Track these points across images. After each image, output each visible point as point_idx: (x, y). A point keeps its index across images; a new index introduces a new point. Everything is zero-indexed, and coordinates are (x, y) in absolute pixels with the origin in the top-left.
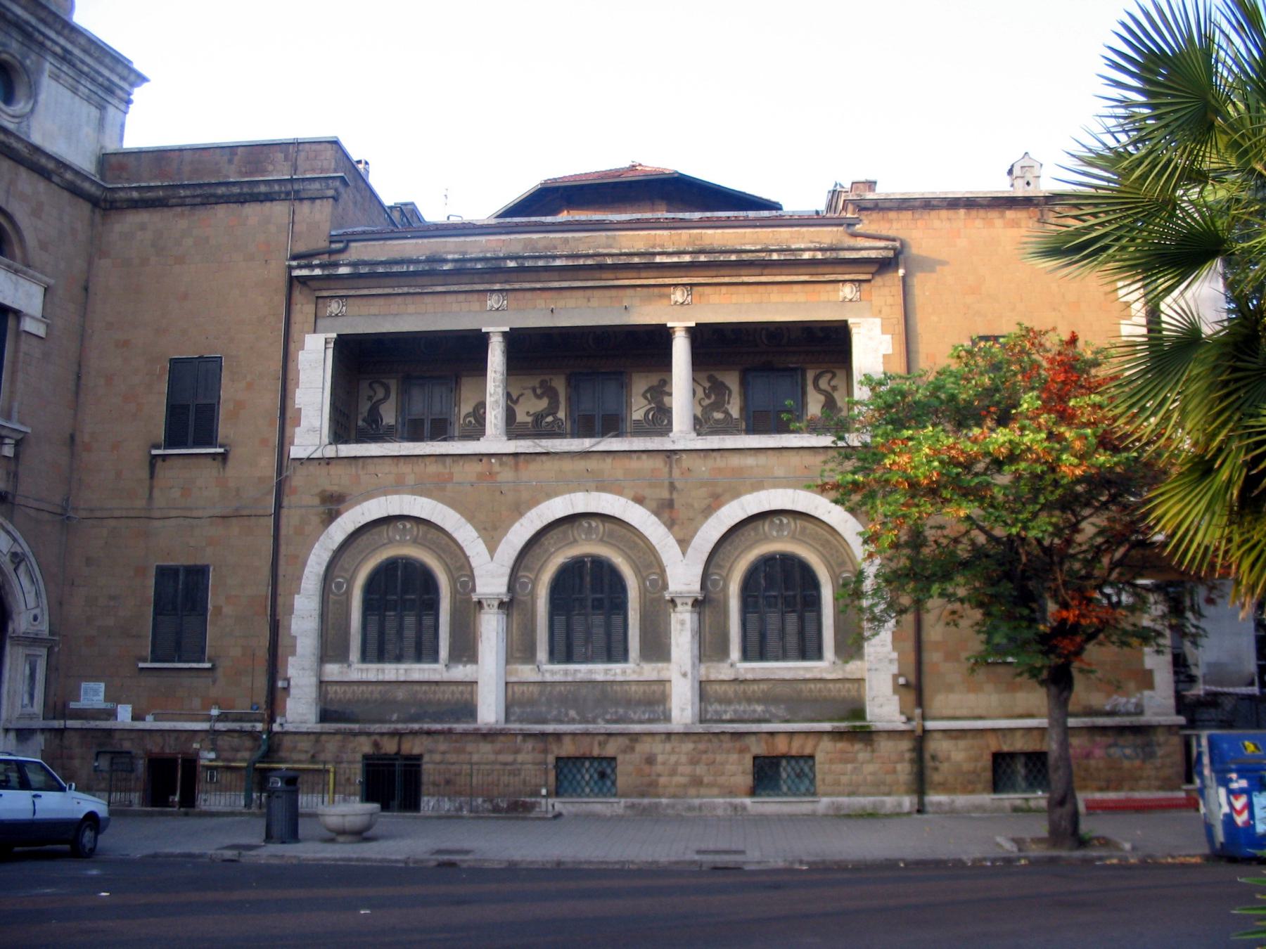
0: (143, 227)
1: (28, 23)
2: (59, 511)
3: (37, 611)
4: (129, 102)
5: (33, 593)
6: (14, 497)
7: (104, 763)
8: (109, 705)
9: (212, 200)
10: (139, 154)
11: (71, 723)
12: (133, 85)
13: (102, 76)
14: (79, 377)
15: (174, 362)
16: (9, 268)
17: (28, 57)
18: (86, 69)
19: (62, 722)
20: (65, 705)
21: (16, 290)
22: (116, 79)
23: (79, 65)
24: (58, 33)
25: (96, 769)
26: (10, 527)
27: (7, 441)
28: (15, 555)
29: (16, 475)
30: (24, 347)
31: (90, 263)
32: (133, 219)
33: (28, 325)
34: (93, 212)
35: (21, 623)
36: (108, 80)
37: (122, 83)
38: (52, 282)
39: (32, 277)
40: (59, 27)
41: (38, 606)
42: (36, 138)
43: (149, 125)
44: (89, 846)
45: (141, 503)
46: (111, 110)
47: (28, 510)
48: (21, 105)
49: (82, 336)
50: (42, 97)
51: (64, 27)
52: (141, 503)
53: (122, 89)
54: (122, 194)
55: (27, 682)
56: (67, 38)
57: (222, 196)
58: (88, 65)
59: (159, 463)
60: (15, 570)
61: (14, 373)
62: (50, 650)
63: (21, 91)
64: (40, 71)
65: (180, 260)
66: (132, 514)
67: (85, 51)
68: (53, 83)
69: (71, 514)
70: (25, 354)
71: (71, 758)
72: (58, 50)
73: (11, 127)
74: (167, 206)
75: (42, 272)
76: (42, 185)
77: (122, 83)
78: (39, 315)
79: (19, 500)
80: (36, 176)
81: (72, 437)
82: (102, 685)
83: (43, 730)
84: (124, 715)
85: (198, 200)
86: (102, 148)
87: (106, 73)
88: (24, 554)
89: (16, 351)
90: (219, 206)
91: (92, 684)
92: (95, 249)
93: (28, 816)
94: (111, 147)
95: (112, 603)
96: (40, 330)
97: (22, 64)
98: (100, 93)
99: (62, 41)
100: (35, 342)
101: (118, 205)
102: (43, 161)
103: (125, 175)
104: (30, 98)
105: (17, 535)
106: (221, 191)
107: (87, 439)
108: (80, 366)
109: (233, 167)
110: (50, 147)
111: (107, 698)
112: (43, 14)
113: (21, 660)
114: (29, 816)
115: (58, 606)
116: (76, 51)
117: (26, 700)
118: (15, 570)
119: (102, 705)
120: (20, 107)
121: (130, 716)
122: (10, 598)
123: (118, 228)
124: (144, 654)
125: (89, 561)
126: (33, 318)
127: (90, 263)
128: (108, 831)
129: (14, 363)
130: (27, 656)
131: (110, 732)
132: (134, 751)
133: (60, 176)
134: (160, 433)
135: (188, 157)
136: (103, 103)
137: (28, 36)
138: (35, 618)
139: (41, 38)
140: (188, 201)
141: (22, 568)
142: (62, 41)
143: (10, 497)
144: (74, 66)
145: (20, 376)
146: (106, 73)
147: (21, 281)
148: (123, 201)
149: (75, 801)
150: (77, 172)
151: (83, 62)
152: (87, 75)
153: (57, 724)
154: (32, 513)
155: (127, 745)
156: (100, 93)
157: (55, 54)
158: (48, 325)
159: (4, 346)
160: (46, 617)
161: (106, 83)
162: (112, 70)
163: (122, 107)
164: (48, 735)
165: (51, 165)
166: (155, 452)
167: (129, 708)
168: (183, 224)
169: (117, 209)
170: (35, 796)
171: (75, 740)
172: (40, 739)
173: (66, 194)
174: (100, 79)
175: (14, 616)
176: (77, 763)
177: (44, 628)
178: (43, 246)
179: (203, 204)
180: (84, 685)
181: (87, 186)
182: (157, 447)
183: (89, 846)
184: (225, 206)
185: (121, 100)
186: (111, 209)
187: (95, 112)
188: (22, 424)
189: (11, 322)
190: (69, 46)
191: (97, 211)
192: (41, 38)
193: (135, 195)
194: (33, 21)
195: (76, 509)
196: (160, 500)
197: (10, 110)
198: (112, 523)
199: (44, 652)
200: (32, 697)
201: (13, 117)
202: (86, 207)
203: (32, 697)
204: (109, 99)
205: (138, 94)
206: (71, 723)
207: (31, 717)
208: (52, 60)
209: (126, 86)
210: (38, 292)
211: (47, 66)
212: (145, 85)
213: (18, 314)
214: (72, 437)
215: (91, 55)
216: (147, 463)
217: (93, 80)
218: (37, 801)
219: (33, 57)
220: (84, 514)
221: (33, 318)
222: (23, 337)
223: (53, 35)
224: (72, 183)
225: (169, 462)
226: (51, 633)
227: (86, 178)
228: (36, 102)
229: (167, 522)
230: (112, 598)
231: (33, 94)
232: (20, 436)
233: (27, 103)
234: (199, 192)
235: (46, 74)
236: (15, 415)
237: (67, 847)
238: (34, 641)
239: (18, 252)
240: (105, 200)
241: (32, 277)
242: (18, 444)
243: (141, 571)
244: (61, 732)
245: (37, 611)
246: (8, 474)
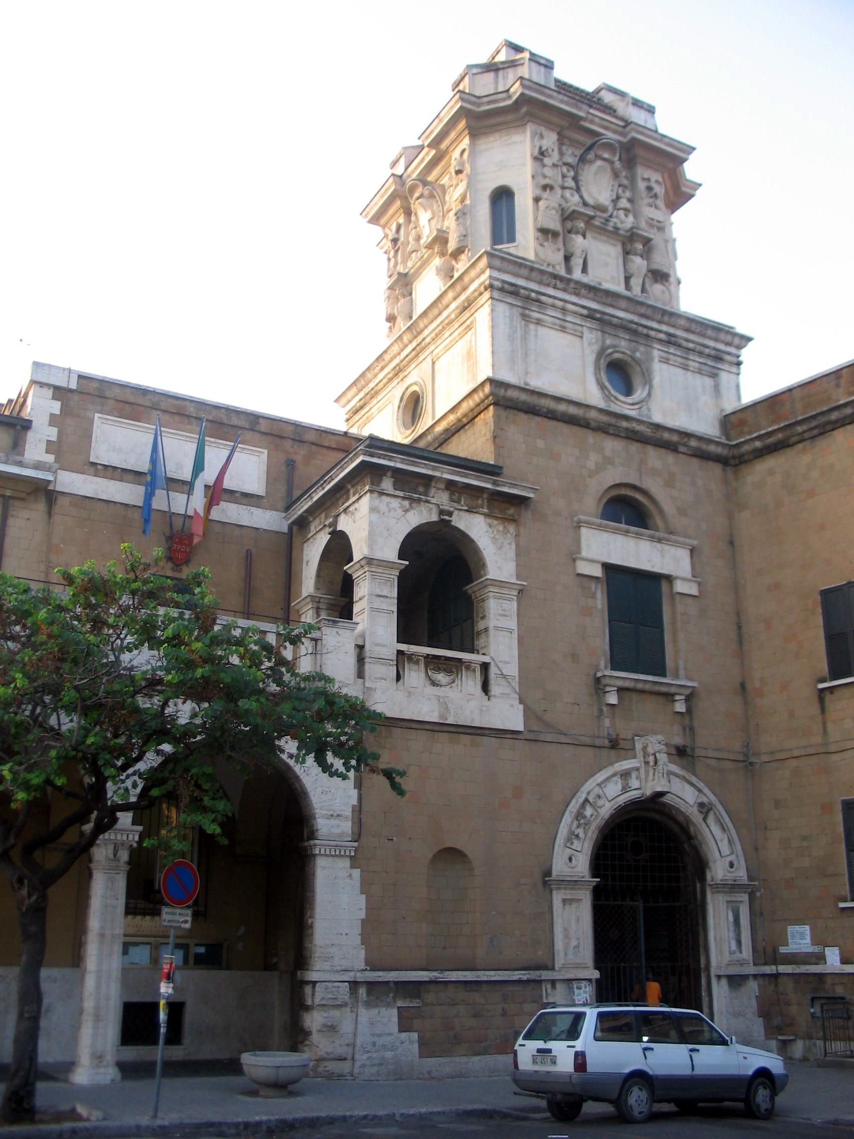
0: (771, 472)
1: (632, 322)
2: (742, 759)
3: (732, 858)
4: (739, 364)
5: (726, 841)
6: (693, 749)
7: (816, 1010)
8: (816, 949)
9: (828, 427)
10: (755, 405)
11: (782, 969)
12: (740, 347)
13: (708, 347)
14: (739, 627)
15: (825, 594)
16: (652, 538)
17: (637, 350)
18: (691, 346)
19: (774, 967)
20: (775, 950)
21: (663, 556)
22: (721, 346)
23: (684, 344)
24: (660, 322)
25: (813, 1015)
26: (694, 779)
27: (677, 697)
28: (701, 805)
29: (692, 729)
30: (680, 608)
31: (730, 517)
32: (761, 467)
33: (680, 587)
34: (724, 470)
35: (718, 871)
36: (715, 349)
37: (728, 349)
38: (695, 543)
39: (676, 542)
40: (659, 317)
41: (732, 853)
42: (658, 418)
43: (761, 376)
44: (764, 1106)
45: (817, 739)
46: (724, 377)
47: (708, 761)
48: (639, 392)
49: (736, 588)
50: (656, 381)
51: (663, 315)
52: (817, 739)
53: (729, 354)
54: (747, 448)
55: (732, 928)
56: (668, 324)
57: (836, 421)
58: (693, 342)
59: (827, 696)
60: (705, 819)
61: (674, 633)
62: (752, 896)
63: (637, 381)
64: (650, 359)
65: (811, 493)
66: (812, 751)
67: (687, 330)
68: (665, 366)
69: (753, 759)
70: (682, 614)
71: (788, 1004)
72: (662, 336)
73: (632, 413)
74: (789, 446)
75: (685, 536)
76: (670, 458)
77: (728, 349)
78: (689, 576)
79: (698, 752)
80: (663, 451)
81: (743, 686)
82: (807, 927)
83: (755, 976)
84: (833, 956)
85: (816, 432)
86: (722, 411)
87: (712, 344)
88: (711, 804)
89: (674, 612)
90: (836, 432)
91: (797, 928)
92: (733, 503)
93: (687, 1071)
94: (730, 407)
95: (805, 844)
96: (693, 590)
97: (633, 358)
98: (710, 363)
99: (664, 328)
100: (689, 601)
101: (746, 458)
102: (666, 436)
103: (746, 429)
104: (645, 384)
105: (701, 785)
106: (834, 416)
107: (757, 685)
108: (738, 615)
109: (841, 390)
110: (670, 423)
111: (814, 942)
112: (643, 310)
113: (722, 906)
114: (687, 1071)
115: (753, 852)
116: (679, 333)
117: (734, 946)
118: (705, 819)
119: (810, 949)
120: (639, 394)
121: (838, 959)
122: (704, 847)
123: (749, 479)
124: (843, 893)
125: (777, 804)
126: (683, 579)
127: (730, 517)
128: (788, 1088)
129: (674, 622)
130: (728, 902)
131: (821, 976)
132: (848, 997)
133: (685, 445)
134: (824, 667)
135: (797, 394)
136: (714, 371)
137: (635, 332)
138: (731, 865)
139: (645, 331)
140: (806, 435)
141: (711, 819)
142: (664, 328)
143: (688, 750)
144: (680, 346)
145: (681, 635)
146: (712, 344)
147: (667, 547)
148: (749, 453)
149: (741, 1056)
150: (700, 438)
151: (687, 340)
152: (693, 350)
153: (769, 969)
154: (713, 762)
155: (840, 991)
156: (710, 363)
157: (660, 341)
158: (699, 584)
159: (661, 611)
160: (743, 863)
161: (713, 353)
162: (716, 340)
163: (734, 369)
164: (761, 981)
165: (675, 438)
166: (821, 686)
167: (836, 950)
168: (806, 459)
169: (746, 462)
170: (692, 1050)
171: (788, 986)
172: (753, 986)
173: (695, 461)
174: (707, 351)
175: (711, 864)
176: (794, 1009)
177: (741, 874)
178: (682, 512)
179: (821, 434)
180: (790, 929)
181: (712, 448)
182: (823, 680)
183: (764, 1106)
184: (841, 429)
185: (731, 363)
186: (740, 463)
187: (708, 382)
188: (690, 679)
189: (664, 586)
190: (672, 330)
191: (728, 469)
192: (645, 331)
193: (758, 444)
194: (636, 319)
195: (758, 754)
196: (834, 734)
197: (629, 400)
198: (794, 763)
199: (745, 897)
200: (739, 943)
201: (633, 404)
202: (716, 469)
203: (739, 943)
204: (719, 366)
205: (746, 354)
206: (782, 969)
207: (741, 963)
208: (659, 347)
209: (732, 350)
210: (683, 555)
211: (656, 353)
212: (751, 343)
213: (669, 578)
214: (743, 686)
215: (693, 332)
216: (817, 698)
217: (701, 354)
218: (694, 1055)
219: (642, 349)
220: (765, 758)
221: (683, 579)
222: (677, 597)
223: (655, 325)
224: (698, 449)
225: (837, 693)
226: (750, 878)
227: (709, 441)
228: (651, 387)
229: (844, 755)
230: (804, 838)
231: (648, 380)
232: (688, 692)
233: (643, 389)
234: (814, 423)
235: (656, 360)
236: (682, 672)
237: (741, 1105)
238: (734, 887)
239: (660, 523)
240: (734, 457)
241: (676, 542)
242: (688, 699)
243: (827, 808)
244: (776, 976)
245: (732, 858)
246: (684, 729)
